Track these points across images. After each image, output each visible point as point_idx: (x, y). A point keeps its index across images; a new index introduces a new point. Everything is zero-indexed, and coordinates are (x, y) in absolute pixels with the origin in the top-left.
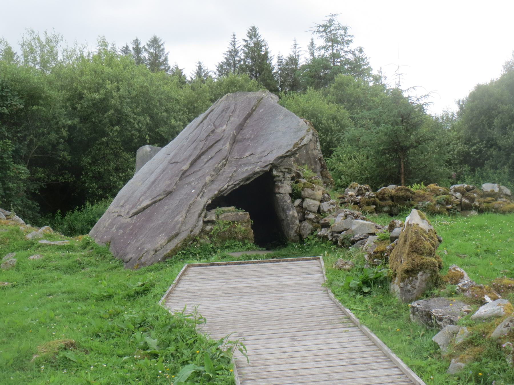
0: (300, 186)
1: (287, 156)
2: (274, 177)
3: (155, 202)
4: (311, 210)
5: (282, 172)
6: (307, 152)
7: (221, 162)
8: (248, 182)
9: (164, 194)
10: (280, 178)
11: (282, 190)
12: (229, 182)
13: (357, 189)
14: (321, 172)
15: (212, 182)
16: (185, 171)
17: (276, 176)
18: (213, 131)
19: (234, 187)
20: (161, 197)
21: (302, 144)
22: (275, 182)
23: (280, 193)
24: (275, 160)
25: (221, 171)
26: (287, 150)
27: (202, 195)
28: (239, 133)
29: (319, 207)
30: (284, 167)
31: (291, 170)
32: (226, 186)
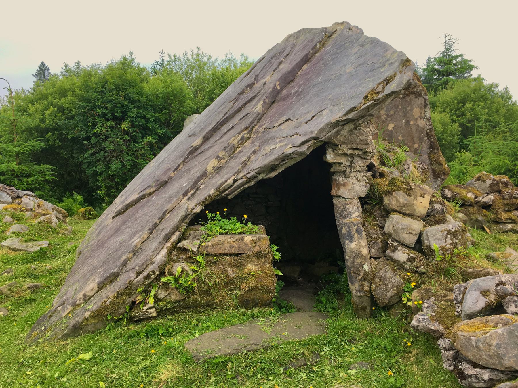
0: (383, 184)
1: (347, 122)
2: (330, 165)
3: (143, 197)
4: (402, 239)
5: (345, 155)
6: (408, 122)
7: (240, 133)
8: (272, 175)
9: (155, 186)
10: (342, 168)
11: (343, 192)
12: (238, 172)
13: (488, 182)
14: (429, 155)
15: (218, 169)
16: (197, 148)
17: (334, 163)
18: (251, 86)
19: (246, 183)
20: (152, 190)
21: (387, 91)
22: (333, 174)
23: (339, 197)
24: (322, 130)
25: (238, 150)
26: (348, 108)
27: (193, 195)
28: (285, 87)
29: (420, 235)
30: (349, 146)
31: (365, 153)
32: (230, 181)
